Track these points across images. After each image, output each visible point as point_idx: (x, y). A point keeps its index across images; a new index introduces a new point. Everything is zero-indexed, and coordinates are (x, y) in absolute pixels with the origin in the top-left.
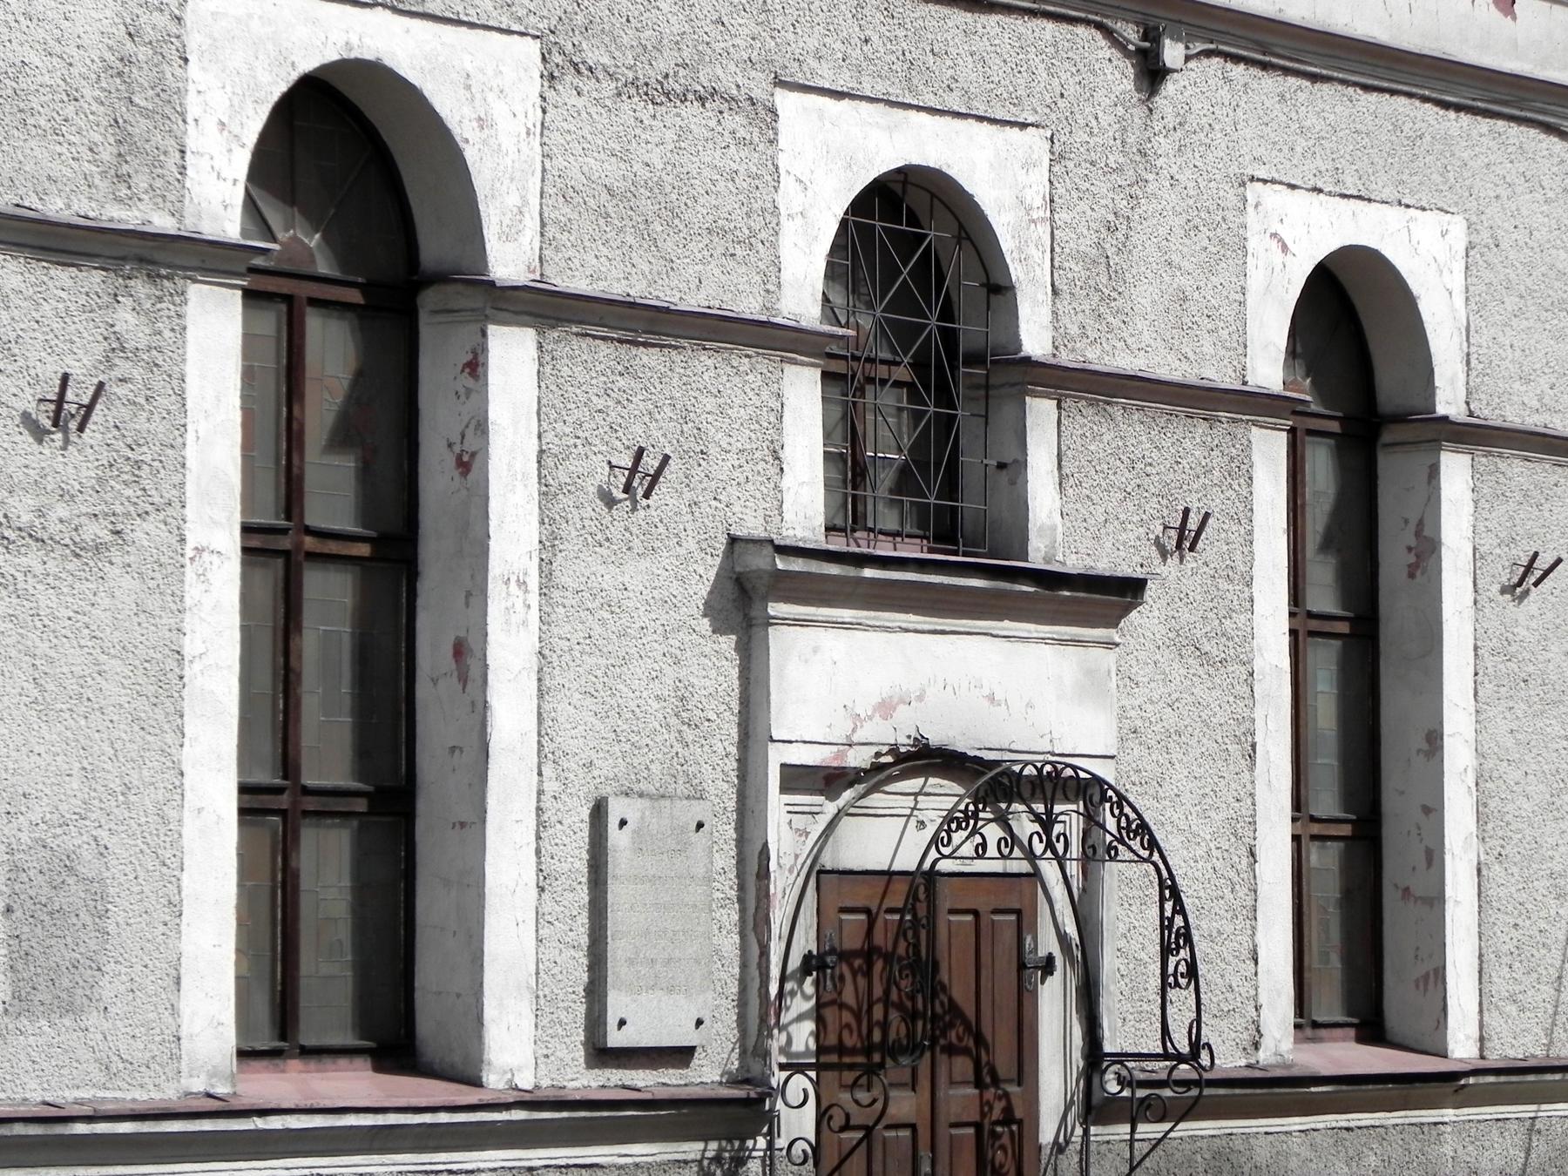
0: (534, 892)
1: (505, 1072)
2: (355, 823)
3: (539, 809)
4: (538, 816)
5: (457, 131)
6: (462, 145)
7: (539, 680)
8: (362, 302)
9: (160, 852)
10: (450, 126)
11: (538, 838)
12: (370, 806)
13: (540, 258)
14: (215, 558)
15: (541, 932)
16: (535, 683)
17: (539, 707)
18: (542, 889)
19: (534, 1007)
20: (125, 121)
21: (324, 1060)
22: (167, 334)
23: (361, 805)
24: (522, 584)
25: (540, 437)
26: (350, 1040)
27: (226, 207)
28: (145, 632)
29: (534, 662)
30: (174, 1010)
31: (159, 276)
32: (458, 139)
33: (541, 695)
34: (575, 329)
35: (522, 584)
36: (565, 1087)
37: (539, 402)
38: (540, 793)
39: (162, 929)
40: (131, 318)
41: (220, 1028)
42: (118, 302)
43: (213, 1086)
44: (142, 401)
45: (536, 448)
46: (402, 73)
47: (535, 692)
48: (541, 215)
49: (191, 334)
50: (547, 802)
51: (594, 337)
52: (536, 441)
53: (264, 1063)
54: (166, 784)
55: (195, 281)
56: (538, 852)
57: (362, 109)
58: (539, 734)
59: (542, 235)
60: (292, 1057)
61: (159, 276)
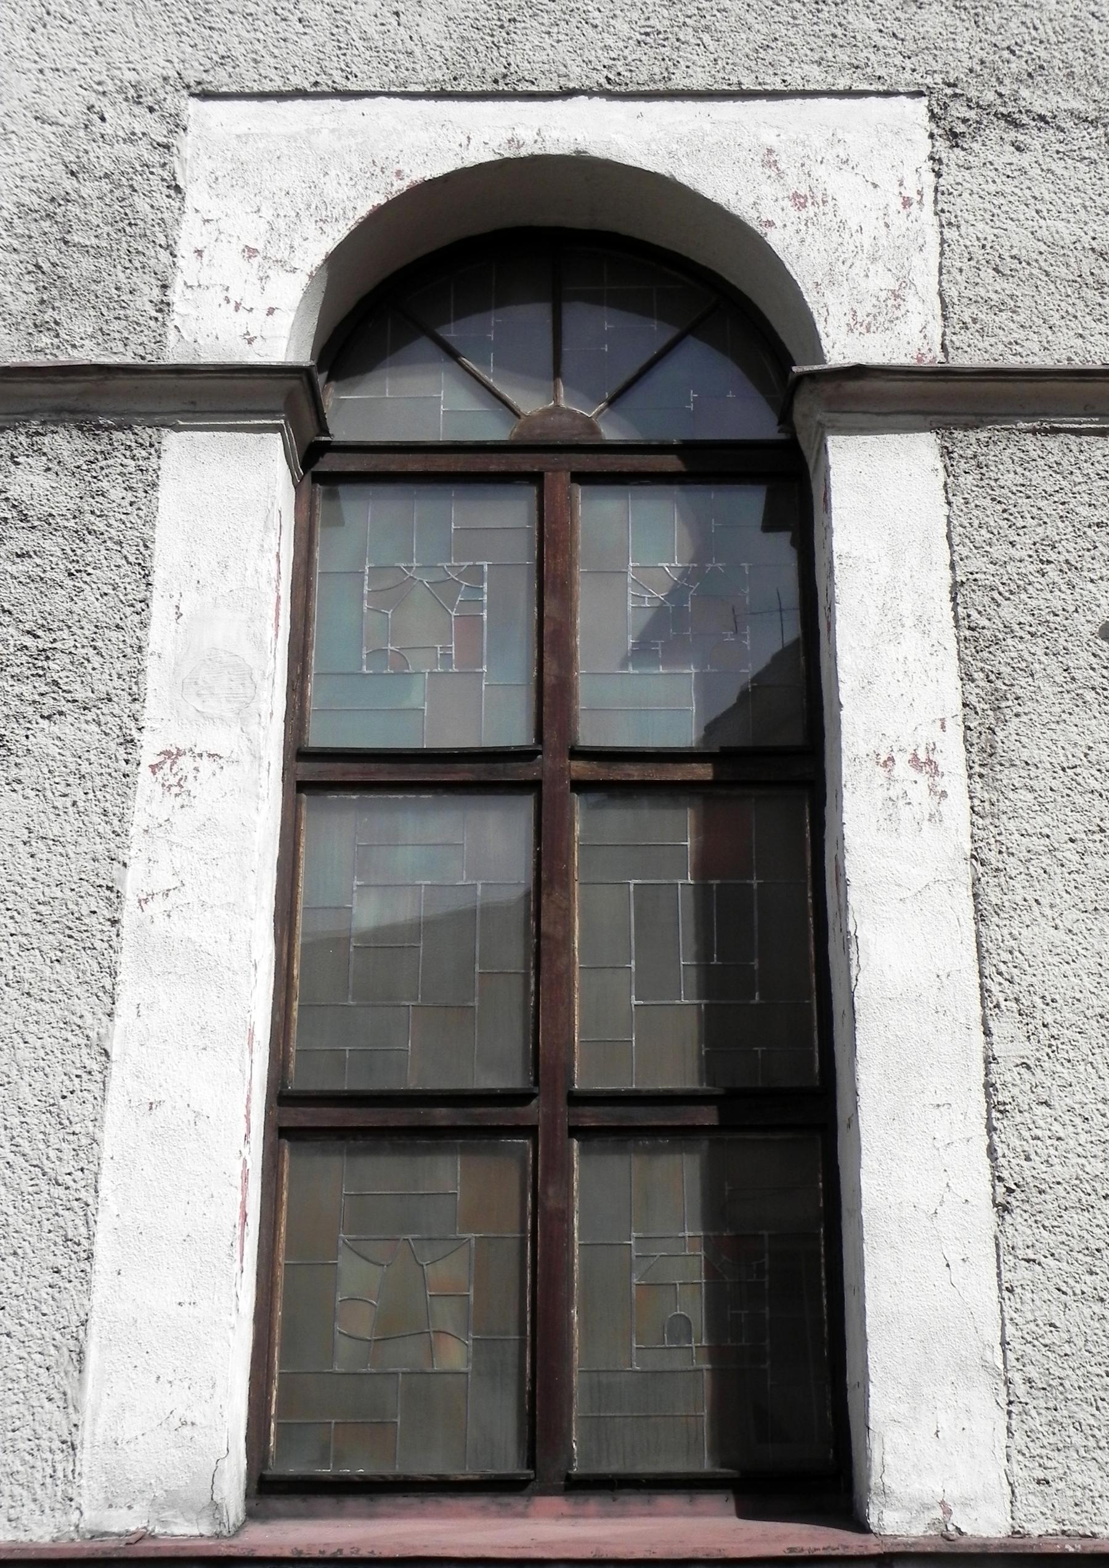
0: (991, 1214)
1: (926, 1507)
2: (705, 1145)
3: (989, 1086)
4: (988, 1095)
5: (749, 216)
6: (760, 230)
7: (975, 896)
8: (684, 470)
9: (47, 1165)
10: (737, 212)
11: (991, 1129)
12: (721, 1116)
13: (943, 346)
14: (205, 764)
15: (1006, 1276)
16: (970, 902)
17: (978, 935)
18: (1003, 1208)
19: (1003, 1399)
20: (54, 265)
21: (621, 1498)
22: (116, 494)
23: (708, 1116)
24: (924, 764)
25: (952, 566)
26: (705, 1465)
27: (250, 342)
28: (40, 865)
29: (965, 872)
30: (69, 1403)
31: (99, 427)
32: (754, 224)
33: (980, 917)
34: (1022, 425)
35: (924, 764)
36: (1094, 1536)
37: (949, 523)
38: (989, 1060)
39: (49, 1277)
40: (42, 482)
41: (186, 1431)
42: (17, 464)
43: (164, 1523)
44: (61, 577)
45: (949, 581)
46: (630, 162)
47: (971, 913)
48: (940, 294)
49: (166, 493)
50: (1004, 1073)
51: (1078, 433)
52: (948, 573)
53: (480, 1501)
54: (69, 1069)
55: (178, 429)
56: (991, 1151)
57: (677, 250)
58: (982, 975)
59: (945, 318)
60: (544, 1492)
61: (99, 427)
